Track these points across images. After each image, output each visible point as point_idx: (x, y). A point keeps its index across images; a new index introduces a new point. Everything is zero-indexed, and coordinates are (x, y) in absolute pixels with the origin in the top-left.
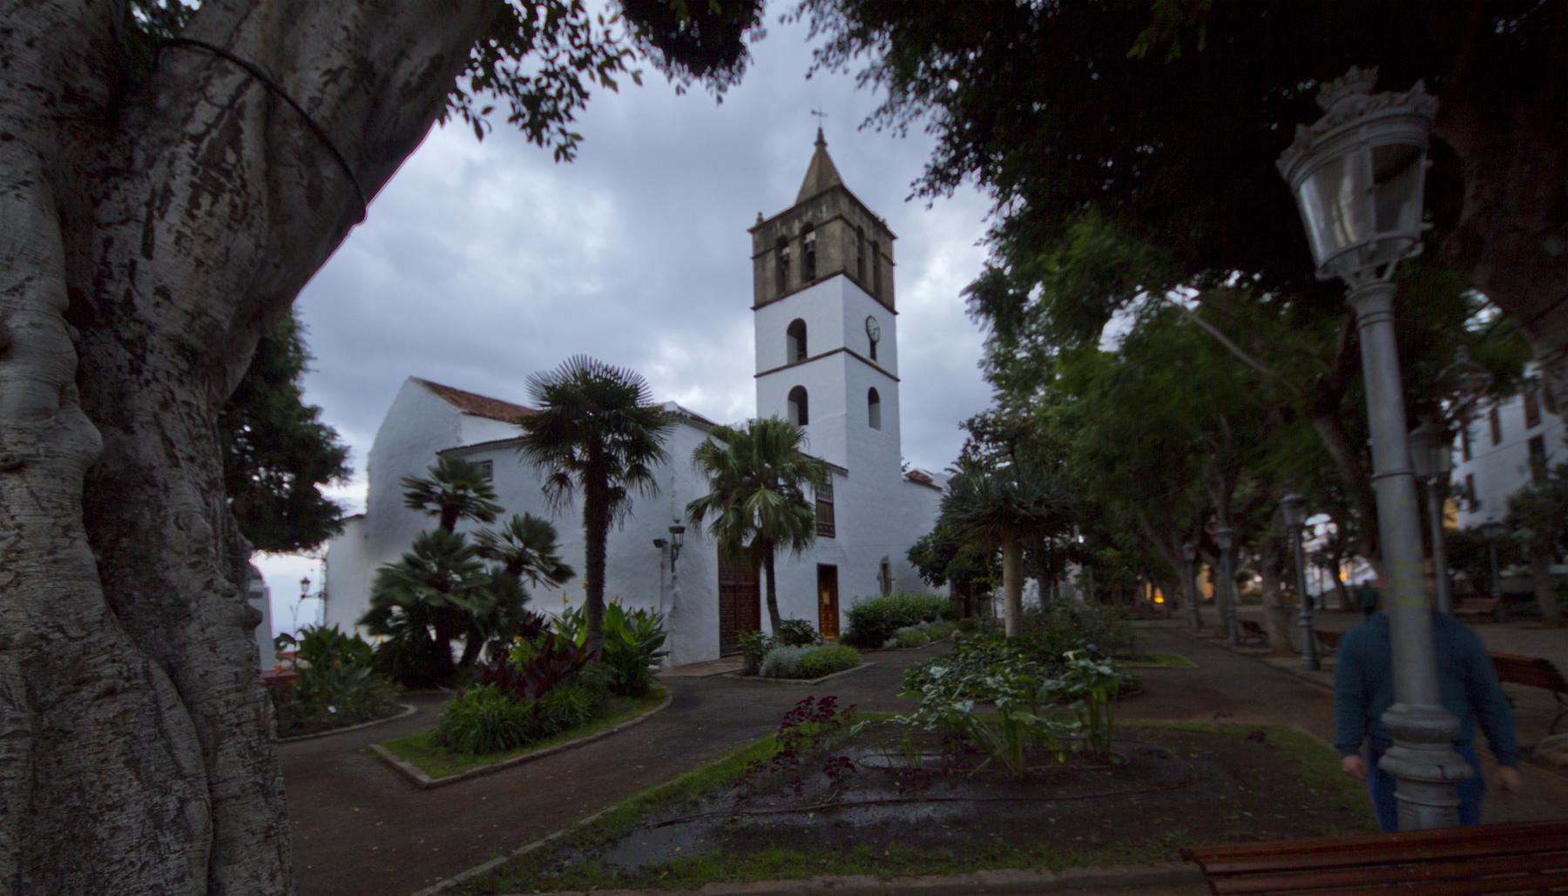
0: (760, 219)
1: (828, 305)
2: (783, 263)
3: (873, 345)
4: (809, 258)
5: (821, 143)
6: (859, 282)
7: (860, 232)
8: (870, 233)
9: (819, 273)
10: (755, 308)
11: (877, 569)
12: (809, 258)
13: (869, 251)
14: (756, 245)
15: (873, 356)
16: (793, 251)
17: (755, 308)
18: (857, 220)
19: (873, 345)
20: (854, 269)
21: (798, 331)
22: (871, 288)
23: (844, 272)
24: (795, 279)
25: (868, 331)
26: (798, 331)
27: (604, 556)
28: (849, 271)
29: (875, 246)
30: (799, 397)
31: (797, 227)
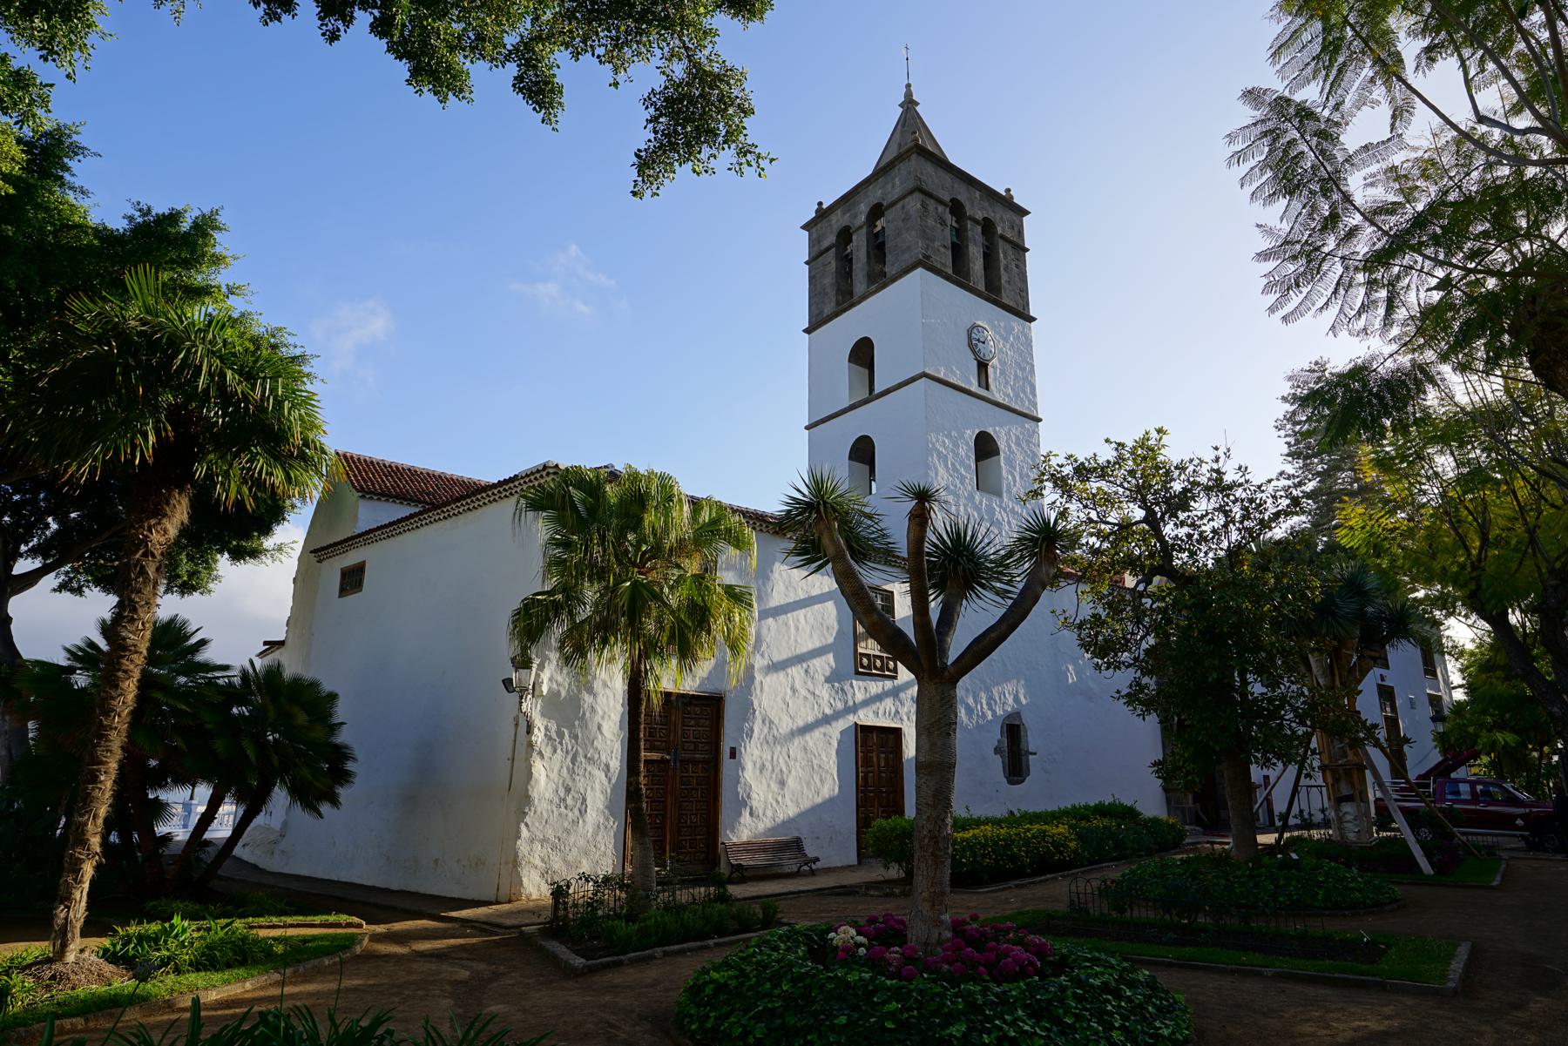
0: (1407, 740)
1: (915, 311)
2: (846, 261)
3: (983, 366)
4: (878, 248)
5: (909, 104)
6: (958, 275)
7: (956, 208)
8: (977, 210)
9: (890, 269)
10: (807, 331)
11: (996, 735)
12: (878, 248)
13: (975, 232)
14: (812, 243)
15: (984, 381)
16: (859, 246)
17: (807, 331)
18: (946, 189)
19: (983, 366)
20: (945, 259)
21: (863, 353)
22: (981, 287)
23: (926, 263)
24: (859, 286)
25: (970, 338)
26: (863, 353)
27: (950, 790)
28: (937, 261)
29: (988, 226)
30: (863, 452)
31: (863, 208)
